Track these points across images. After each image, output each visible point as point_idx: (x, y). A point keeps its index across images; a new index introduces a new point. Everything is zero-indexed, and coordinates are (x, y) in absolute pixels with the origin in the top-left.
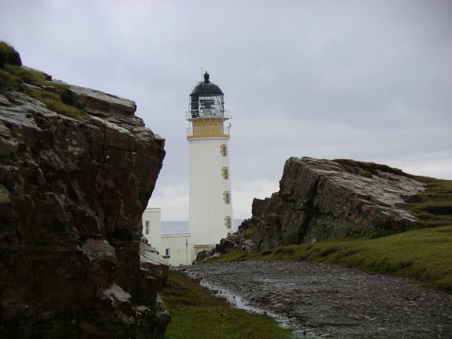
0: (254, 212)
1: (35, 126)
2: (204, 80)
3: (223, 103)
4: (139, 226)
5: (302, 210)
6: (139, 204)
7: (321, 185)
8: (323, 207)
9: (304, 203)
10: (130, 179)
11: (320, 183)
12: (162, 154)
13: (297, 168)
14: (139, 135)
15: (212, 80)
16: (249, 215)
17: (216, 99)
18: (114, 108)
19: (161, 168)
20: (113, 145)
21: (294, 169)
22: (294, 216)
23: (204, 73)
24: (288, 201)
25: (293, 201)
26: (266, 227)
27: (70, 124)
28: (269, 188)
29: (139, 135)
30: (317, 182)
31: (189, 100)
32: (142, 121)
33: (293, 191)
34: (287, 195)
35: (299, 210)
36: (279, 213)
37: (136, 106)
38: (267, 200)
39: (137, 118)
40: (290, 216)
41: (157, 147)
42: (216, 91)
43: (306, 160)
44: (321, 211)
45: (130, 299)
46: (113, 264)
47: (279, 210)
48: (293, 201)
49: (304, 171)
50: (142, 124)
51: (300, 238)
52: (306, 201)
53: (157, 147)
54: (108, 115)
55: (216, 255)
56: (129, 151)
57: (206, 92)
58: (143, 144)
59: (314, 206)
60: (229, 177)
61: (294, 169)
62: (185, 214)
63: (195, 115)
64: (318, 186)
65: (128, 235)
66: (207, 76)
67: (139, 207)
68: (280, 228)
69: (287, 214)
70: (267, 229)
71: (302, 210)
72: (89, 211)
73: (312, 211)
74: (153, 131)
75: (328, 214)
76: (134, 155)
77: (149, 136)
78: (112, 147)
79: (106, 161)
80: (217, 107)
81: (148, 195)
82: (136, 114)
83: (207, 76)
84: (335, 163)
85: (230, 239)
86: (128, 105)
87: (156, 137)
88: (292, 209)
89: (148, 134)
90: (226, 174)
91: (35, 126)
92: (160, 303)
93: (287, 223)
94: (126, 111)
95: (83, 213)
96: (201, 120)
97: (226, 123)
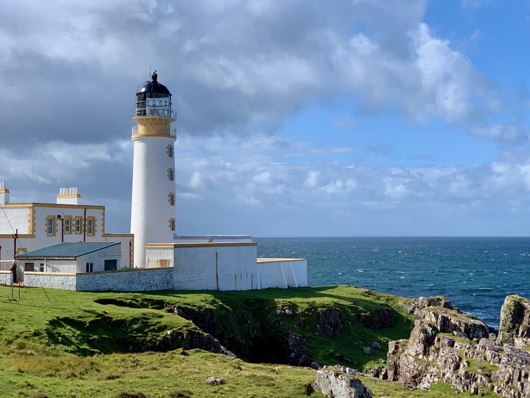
2: (151, 80)
3: (170, 104)
60: (175, 203)
66: (155, 77)
83: (155, 77)
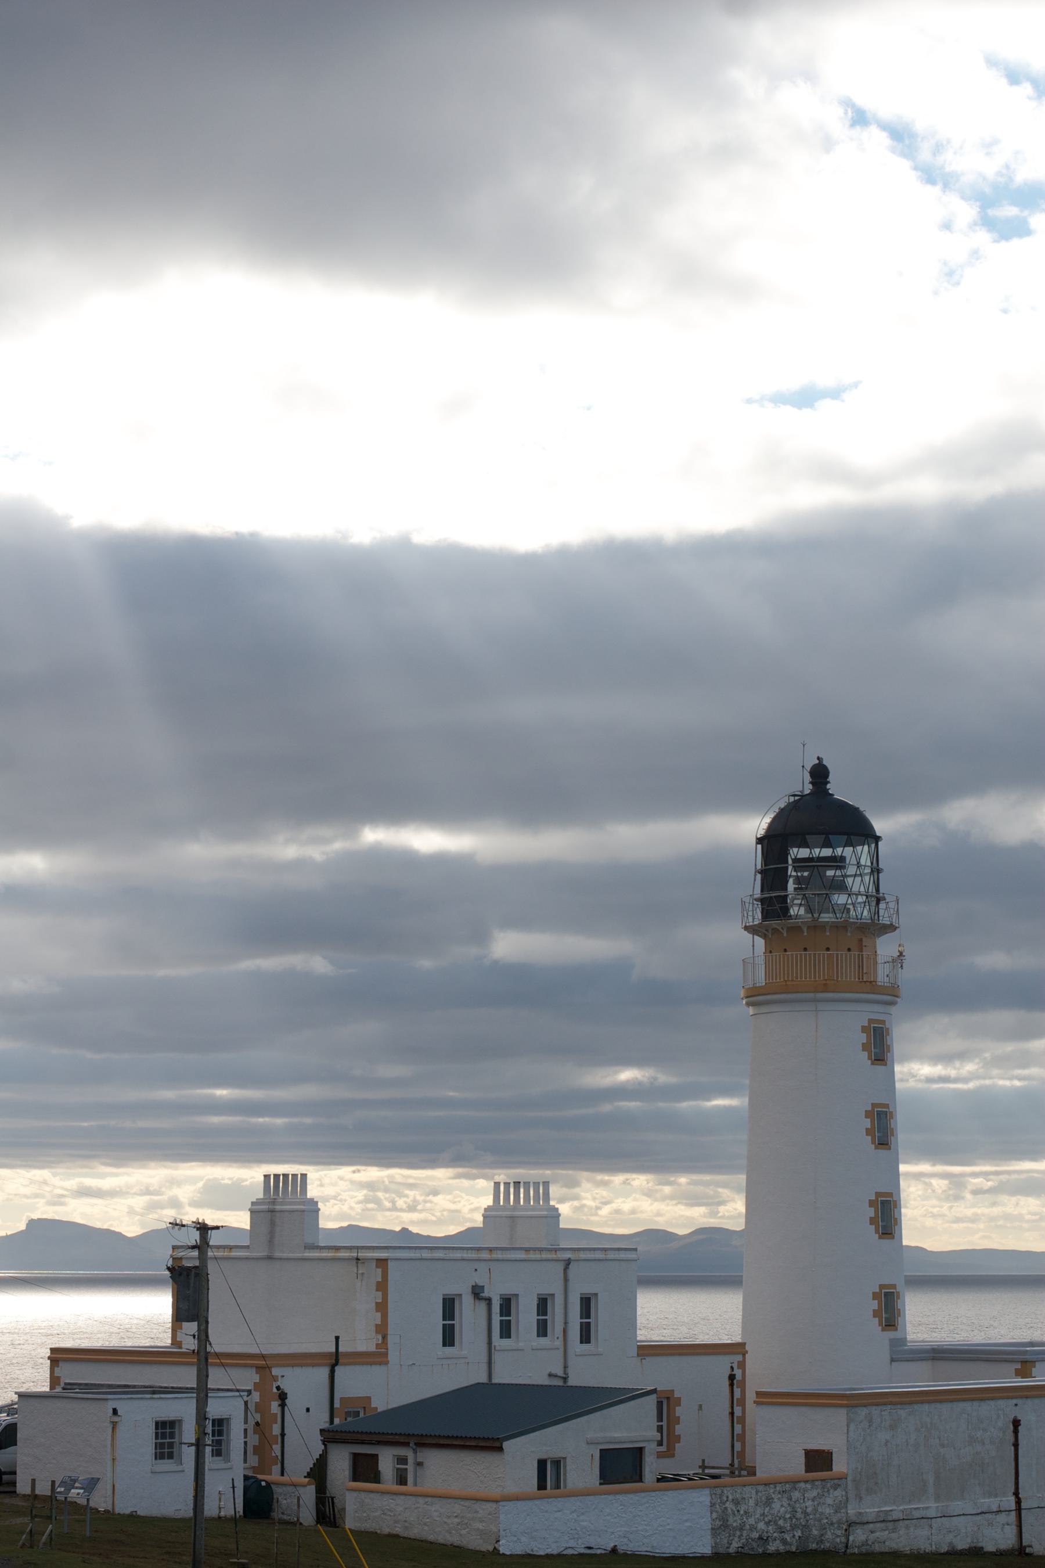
3: (876, 870)
15: (839, 789)
66: (820, 774)
83: (820, 774)
96: (796, 929)
97: (885, 947)
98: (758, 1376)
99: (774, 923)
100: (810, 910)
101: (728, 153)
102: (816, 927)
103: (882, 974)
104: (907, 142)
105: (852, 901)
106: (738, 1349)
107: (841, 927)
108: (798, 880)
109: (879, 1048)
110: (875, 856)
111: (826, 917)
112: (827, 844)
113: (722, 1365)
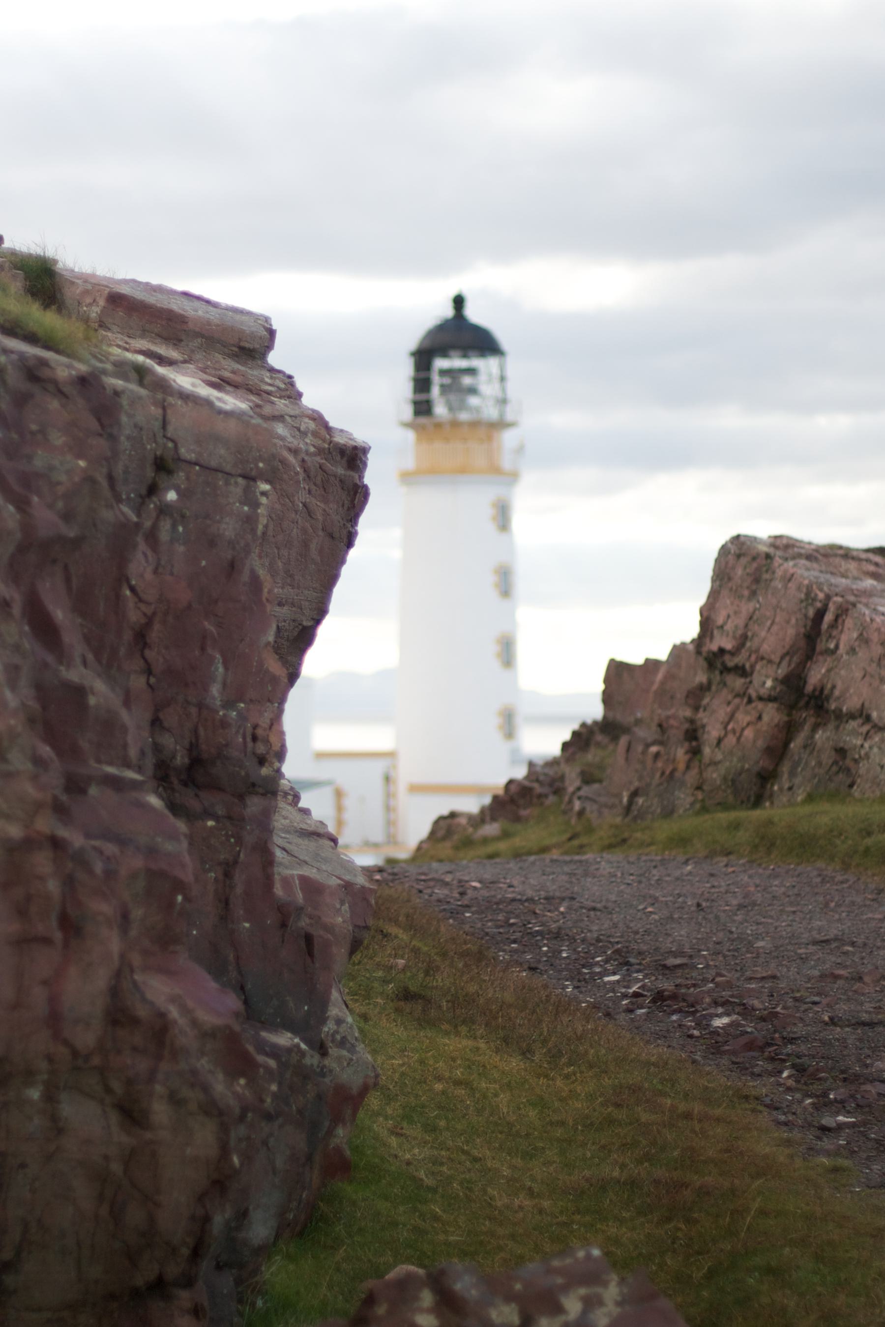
0: (608, 698)
1: (216, 634)
3: (503, 379)
4: (276, 747)
5: (771, 699)
6: (274, 666)
7: (834, 625)
8: (837, 693)
9: (775, 680)
10: (245, 577)
11: (829, 617)
12: (357, 497)
13: (758, 569)
14: (280, 429)
15: (474, 314)
16: (595, 711)
17: (487, 366)
18: (203, 336)
19: (350, 544)
20: (192, 457)
21: (744, 567)
22: (742, 718)
23: (453, 293)
24: (726, 670)
25: (741, 671)
26: (654, 749)
27: (45, 373)
28: (664, 625)
29: (280, 429)
30: (820, 614)
31: (406, 369)
32: (292, 384)
33: (744, 639)
34: (722, 651)
35: (760, 699)
36: (696, 708)
37: (272, 333)
38: (651, 665)
39: (272, 370)
40: (732, 717)
41: (340, 471)
42: (483, 343)
43: (785, 546)
44: (833, 706)
45: (237, 1015)
46: (179, 886)
47: (696, 696)
48: (741, 671)
49: (783, 578)
50: (291, 392)
51: (758, 786)
52: (781, 672)
53: (340, 471)
54: (174, 354)
55: (491, 829)
56: (245, 477)
57: (459, 337)
58: (291, 458)
59: (809, 688)
61: (744, 567)
62: (420, 694)
63: (422, 408)
64: (825, 626)
65: (227, 772)
66: (459, 302)
67: (274, 680)
68: (695, 752)
69: (722, 713)
70: (657, 755)
71: (771, 699)
72: (100, 686)
73: (803, 700)
74: (327, 418)
75: (852, 716)
76: (264, 494)
77: (315, 434)
78: (189, 462)
79: (164, 510)
80: (488, 388)
81: (303, 638)
82: (274, 359)
83: (459, 302)
84: (871, 556)
85: (537, 781)
86: (249, 326)
87: (339, 439)
88: (737, 695)
89: (312, 425)
90: (505, 582)
91: (216, 634)
92: (339, 1022)
93: (719, 741)
94: (242, 345)
95: (79, 692)
96: (438, 426)
97: (508, 438)
98: (406, 774)
99: (423, 420)
100: (451, 409)
101: (27, 303)
102: (455, 424)
103: (506, 463)
104: (852, 599)
105: (483, 404)
106: (391, 755)
107: (475, 424)
108: (443, 387)
109: (502, 516)
110: (502, 368)
111: (464, 416)
112: (465, 356)
113: (378, 768)
